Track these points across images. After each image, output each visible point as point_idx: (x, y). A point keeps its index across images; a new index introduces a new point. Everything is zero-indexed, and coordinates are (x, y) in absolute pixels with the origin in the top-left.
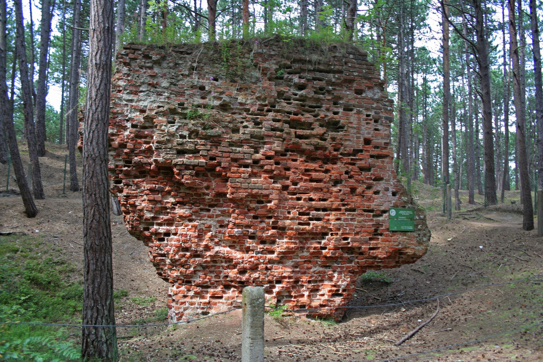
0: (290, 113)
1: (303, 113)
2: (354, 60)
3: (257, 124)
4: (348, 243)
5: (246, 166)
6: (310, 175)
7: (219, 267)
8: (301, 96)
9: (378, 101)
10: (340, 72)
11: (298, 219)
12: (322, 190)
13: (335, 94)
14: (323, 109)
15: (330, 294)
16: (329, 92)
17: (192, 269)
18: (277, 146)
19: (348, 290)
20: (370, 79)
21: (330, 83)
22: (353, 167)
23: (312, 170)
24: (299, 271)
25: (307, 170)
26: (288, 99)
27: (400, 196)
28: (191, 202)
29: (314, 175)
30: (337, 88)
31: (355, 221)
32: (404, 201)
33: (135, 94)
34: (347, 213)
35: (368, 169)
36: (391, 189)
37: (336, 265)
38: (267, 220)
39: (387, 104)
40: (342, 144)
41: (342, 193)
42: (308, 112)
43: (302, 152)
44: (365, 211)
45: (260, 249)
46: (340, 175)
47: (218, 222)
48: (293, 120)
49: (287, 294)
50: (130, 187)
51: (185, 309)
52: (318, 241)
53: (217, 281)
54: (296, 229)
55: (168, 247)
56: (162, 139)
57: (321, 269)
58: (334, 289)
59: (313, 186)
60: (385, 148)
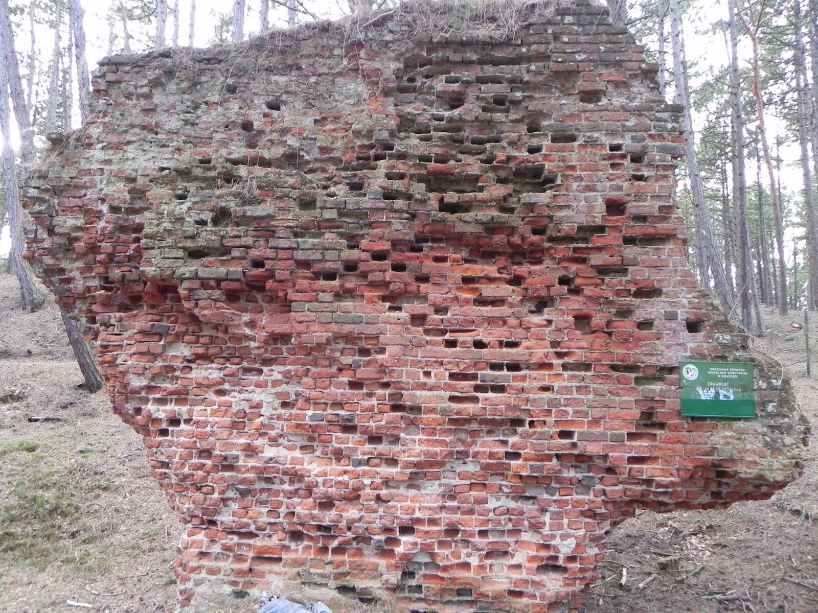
0: (426, 159)
1: (460, 156)
2: (576, 28)
3: (356, 187)
4: (574, 445)
5: (330, 276)
6: (477, 289)
7: (277, 493)
8: (451, 120)
9: (639, 112)
10: (545, 57)
11: (447, 387)
12: (505, 323)
13: (530, 108)
14: (504, 143)
15: (535, 565)
16: (516, 103)
17: (216, 496)
18: (400, 228)
19: (581, 558)
20: (618, 64)
21: (515, 83)
22: (581, 266)
23: (479, 278)
24: (459, 508)
25: (467, 280)
26: (423, 131)
27: (712, 331)
28: (224, 355)
29: (488, 291)
30: (537, 96)
31: (588, 393)
32: (720, 344)
33: (117, 148)
34: (566, 374)
35: (621, 270)
36: (682, 315)
37: (546, 496)
38: (380, 392)
39: (665, 115)
40: (551, 217)
41: (553, 327)
42: (470, 153)
43: (458, 240)
44: (614, 368)
45: (364, 454)
46: (548, 287)
47: (278, 395)
48: (437, 174)
49: (428, 560)
50: (111, 328)
51: (198, 583)
52: (502, 438)
53: (270, 524)
54: (444, 412)
55: (173, 448)
56: (156, 229)
57: (512, 504)
58: (544, 553)
59: (485, 314)
60: (664, 219)
